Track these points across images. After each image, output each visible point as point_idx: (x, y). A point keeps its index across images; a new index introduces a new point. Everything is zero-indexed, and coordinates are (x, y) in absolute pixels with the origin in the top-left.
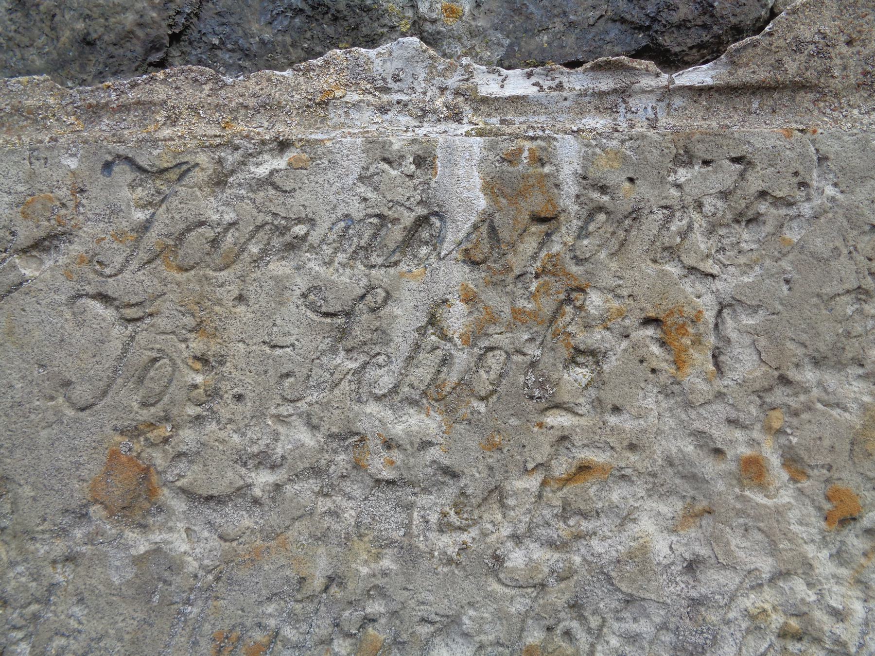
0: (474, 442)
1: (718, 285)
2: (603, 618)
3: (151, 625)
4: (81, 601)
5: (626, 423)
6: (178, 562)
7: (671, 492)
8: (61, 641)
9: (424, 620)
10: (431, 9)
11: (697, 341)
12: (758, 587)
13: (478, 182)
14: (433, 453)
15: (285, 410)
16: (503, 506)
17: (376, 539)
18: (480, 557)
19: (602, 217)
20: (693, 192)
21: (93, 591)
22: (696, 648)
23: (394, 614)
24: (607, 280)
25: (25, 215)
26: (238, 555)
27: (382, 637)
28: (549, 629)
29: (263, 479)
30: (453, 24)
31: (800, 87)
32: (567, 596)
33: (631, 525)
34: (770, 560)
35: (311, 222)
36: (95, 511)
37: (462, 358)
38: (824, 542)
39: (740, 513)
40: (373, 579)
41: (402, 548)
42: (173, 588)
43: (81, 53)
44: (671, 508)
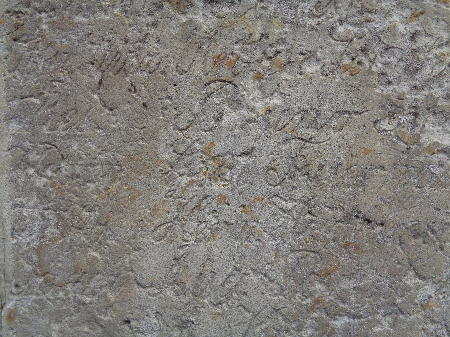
2: (376, 55)
3: (187, 51)
4: (158, 41)
6: (199, 26)
7: (406, 7)
8: (148, 58)
9: (301, 54)
16: (336, 8)
21: (164, 37)
22: (414, 69)
23: (288, 50)
26: (224, 24)
27: (283, 59)
28: (353, 59)
32: (361, 45)
33: (389, 18)
34: (447, 34)
39: (436, 13)
40: (280, 35)
41: (293, 23)
42: (197, 36)
44: (407, 13)
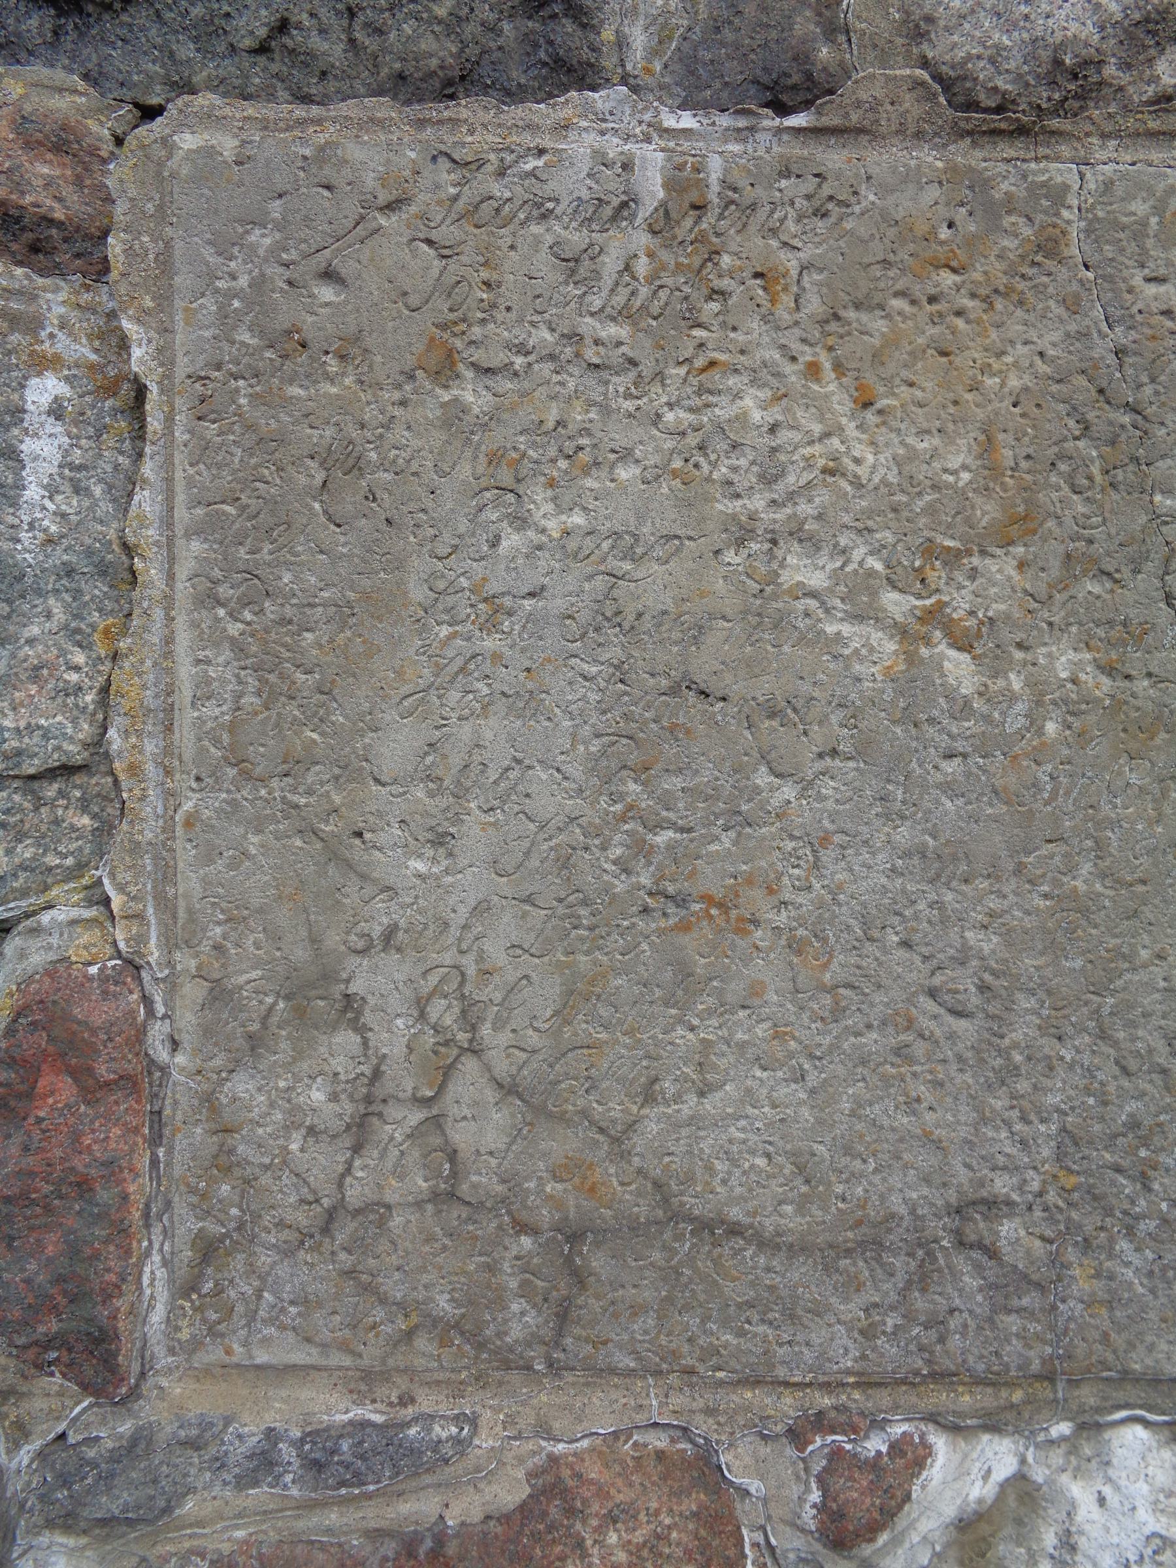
0: (648, 343)
1: (801, 255)
4: (409, 428)
5: (739, 337)
7: (765, 385)
9: (613, 451)
10: (634, 68)
11: (785, 289)
12: (811, 443)
13: (659, 181)
15: (536, 318)
16: (663, 385)
17: (587, 400)
18: (648, 413)
19: (733, 207)
20: (789, 194)
24: (734, 247)
25: (383, 186)
28: (686, 461)
29: (519, 361)
30: (649, 80)
31: (860, 131)
35: (557, 201)
36: (420, 374)
37: (644, 291)
38: (853, 417)
39: (804, 396)
43: (396, 85)
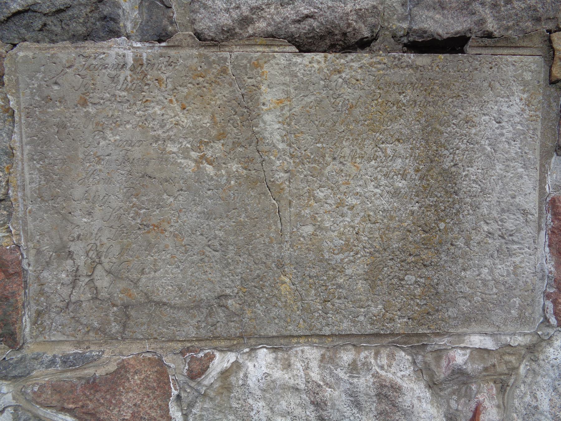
0: (132, 96)
11: (163, 83)
12: (172, 118)
14: (126, 98)
29: (102, 101)
30: (133, 34)
31: (178, 46)
36: (78, 105)
37: (130, 84)
